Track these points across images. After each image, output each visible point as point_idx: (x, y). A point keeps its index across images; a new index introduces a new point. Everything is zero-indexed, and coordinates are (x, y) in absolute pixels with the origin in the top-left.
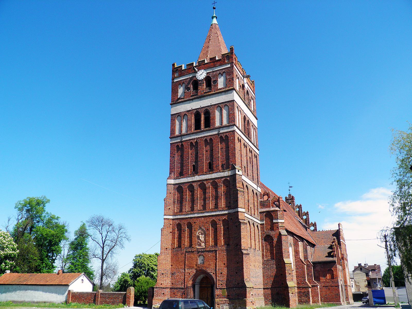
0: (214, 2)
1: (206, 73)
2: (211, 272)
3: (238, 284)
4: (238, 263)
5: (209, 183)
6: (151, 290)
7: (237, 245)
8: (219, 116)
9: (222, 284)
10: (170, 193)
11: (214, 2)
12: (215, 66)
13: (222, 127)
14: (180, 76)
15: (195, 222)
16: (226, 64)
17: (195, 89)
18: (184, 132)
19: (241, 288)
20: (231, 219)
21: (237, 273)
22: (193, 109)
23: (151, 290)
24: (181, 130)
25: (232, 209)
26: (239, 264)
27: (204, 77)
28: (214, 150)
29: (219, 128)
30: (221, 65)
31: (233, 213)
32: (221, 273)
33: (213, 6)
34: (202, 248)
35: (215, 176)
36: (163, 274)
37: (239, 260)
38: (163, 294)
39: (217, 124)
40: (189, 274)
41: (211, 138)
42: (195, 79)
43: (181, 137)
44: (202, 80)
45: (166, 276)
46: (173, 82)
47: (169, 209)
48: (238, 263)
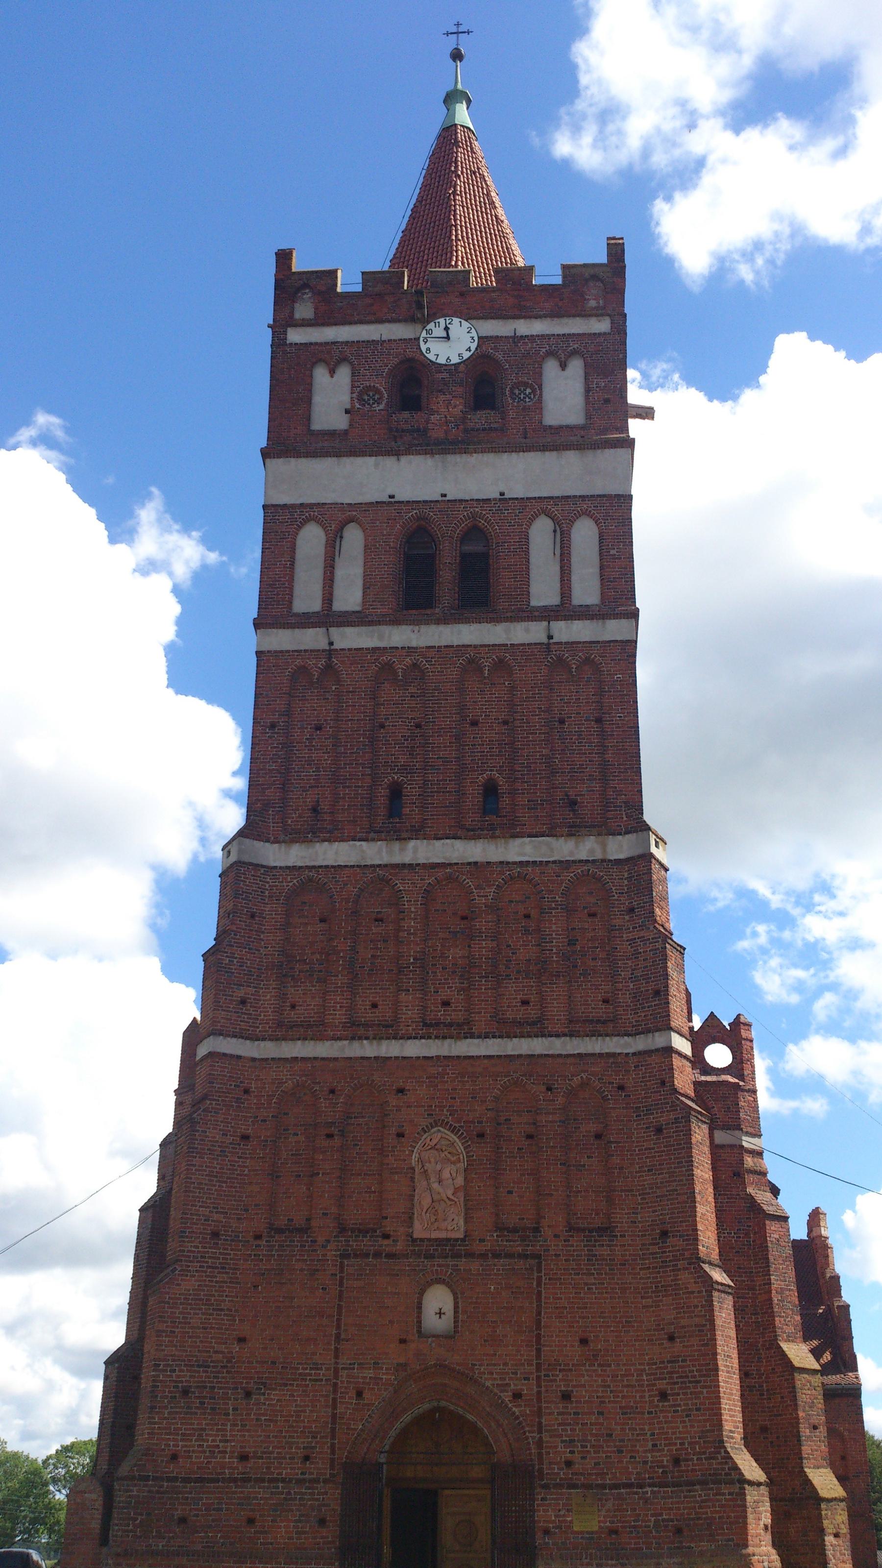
0: (458, 25)
1: (476, 339)
2: (504, 1387)
3: (677, 1461)
4: (671, 1338)
5: (489, 886)
6: (94, 1496)
7: (664, 1234)
8: (549, 542)
9: (569, 1464)
10: (253, 916)
11: (458, 25)
12: (522, 313)
13: (565, 610)
14: (320, 321)
15: (401, 1091)
16: (584, 314)
17: (407, 406)
18: (339, 605)
19: (703, 1483)
20: (621, 1088)
21: (663, 1396)
22: (447, 498)
23: (94, 1496)
24: (328, 598)
25: (629, 1035)
26: (678, 1346)
27: (467, 355)
28: (517, 723)
29: (549, 614)
30: (556, 314)
31: (634, 1054)
32: (566, 1397)
33: (450, 43)
34: (448, 1240)
35: (524, 855)
36: (186, 1392)
37: (683, 1322)
38: (183, 1520)
39: (543, 591)
40: (359, 1394)
41: (501, 661)
42: (409, 353)
43: (545, 623)
44: (451, 369)
45: (202, 1403)
46: (279, 344)
47: (243, 1002)
48: (671, 1338)
